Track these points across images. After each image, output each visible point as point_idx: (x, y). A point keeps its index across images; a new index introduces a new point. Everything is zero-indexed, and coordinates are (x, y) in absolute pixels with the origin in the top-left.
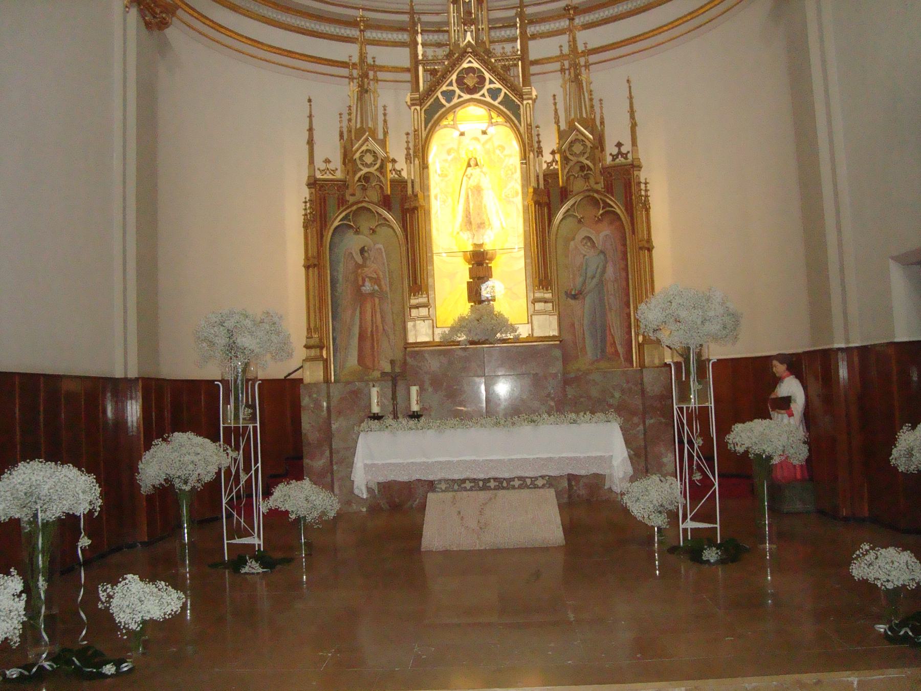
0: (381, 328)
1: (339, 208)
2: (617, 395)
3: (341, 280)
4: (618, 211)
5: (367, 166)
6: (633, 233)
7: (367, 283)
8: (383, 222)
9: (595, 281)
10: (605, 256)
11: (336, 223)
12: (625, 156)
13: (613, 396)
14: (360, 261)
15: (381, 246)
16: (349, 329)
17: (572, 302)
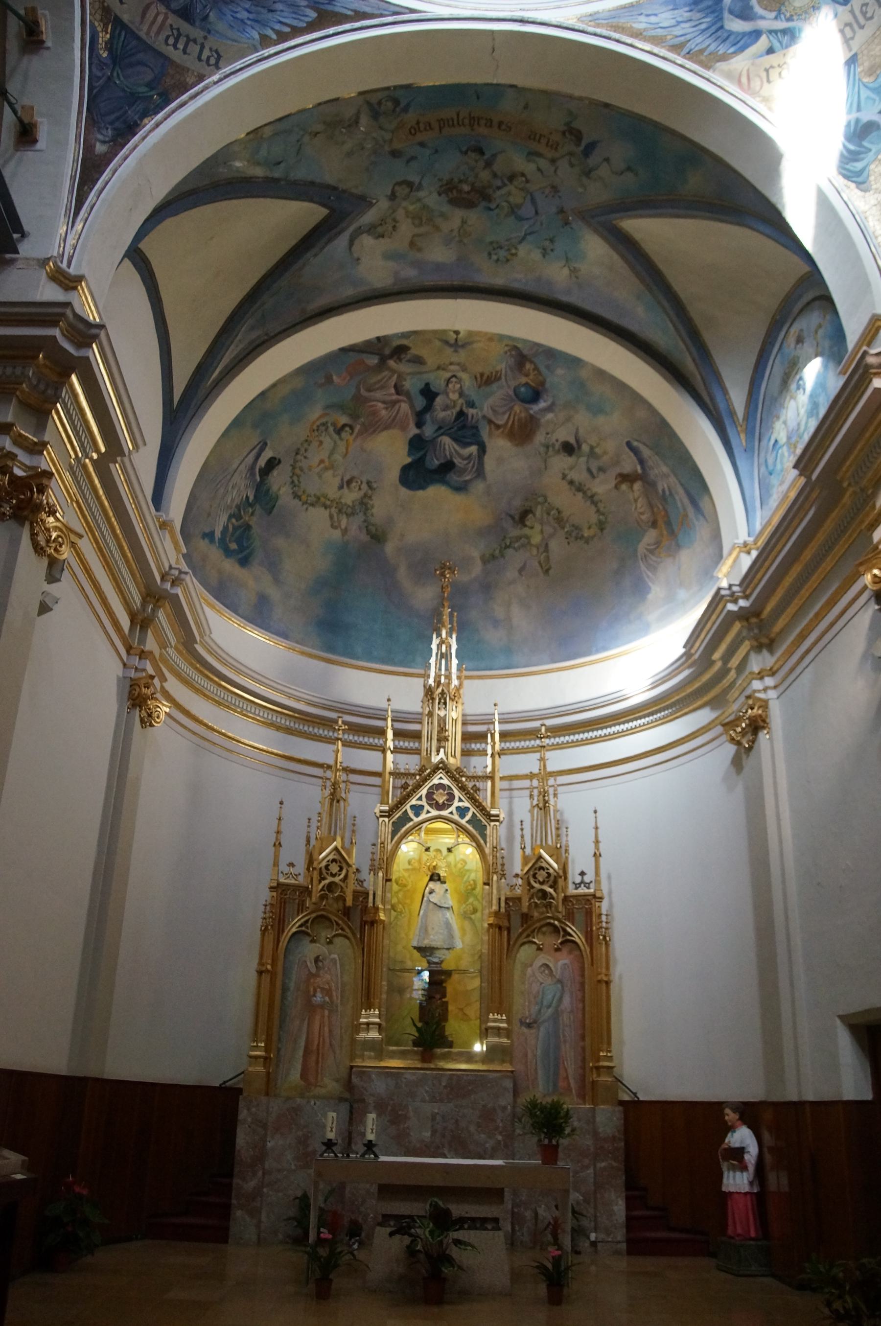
0: (327, 1040)
3: (292, 989)
6: (592, 965)
7: (319, 995)
9: (550, 1011)
11: (294, 930)
14: (314, 970)
15: (336, 956)
17: (525, 1030)
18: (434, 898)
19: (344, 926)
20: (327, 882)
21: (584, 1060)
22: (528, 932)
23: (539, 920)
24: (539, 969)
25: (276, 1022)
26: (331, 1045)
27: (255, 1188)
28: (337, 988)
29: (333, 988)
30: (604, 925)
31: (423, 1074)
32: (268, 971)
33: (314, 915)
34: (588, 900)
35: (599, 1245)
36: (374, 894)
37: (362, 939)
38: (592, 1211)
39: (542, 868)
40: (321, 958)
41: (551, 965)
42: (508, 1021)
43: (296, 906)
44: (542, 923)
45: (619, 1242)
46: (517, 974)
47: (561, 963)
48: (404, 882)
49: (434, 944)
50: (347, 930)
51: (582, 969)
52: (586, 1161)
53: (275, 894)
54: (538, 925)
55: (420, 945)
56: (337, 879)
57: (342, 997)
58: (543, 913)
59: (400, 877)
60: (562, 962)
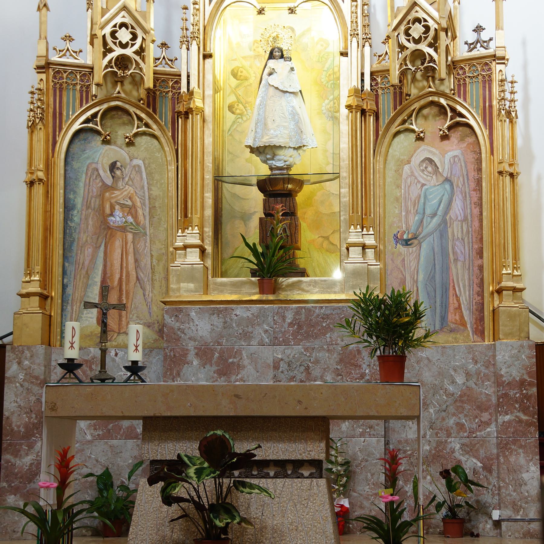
0: (133, 273)
1: (81, 106)
2: (460, 380)
3: (79, 206)
4: (472, 122)
5: (124, 46)
6: (492, 153)
7: (118, 213)
8: (144, 129)
9: (436, 220)
10: (452, 185)
11: (76, 126)
12: (485, 44)
13: (453, 382)
14: (109, 181)
15: (140, 162)
16: (88, 275)
17: (401, 248)
18: (274, 80)
19: (150, 122)
20: (114, 55)
21: (481, 284)
22: (404, 116)
23: (420, 98)
24: (421, 165)
25: (58, 252)
26: (137, 278)
27: (31, 464)
28: (143, 204)
29: (139, 204)
30: (508, 96)
31: (261, 309)
32: (40, 180)
33: (105, 106)
34: (486, 64)
35: (504, 525)
36: (188, 76)
37: (174, 137)
38: (494, 481)
39: (418, 20)
40: (119, 164)
41: (436, 160)
42: (378, 237)
43: (78, 95)
44: (422, 102)
45: (531, 521)
46: (390, 174)
47: (450, 154)
48: (245, 73)
49: (276, 141)
50: (155, 127)
51: (479, 161)
52: (485, 416)
53: (43, 76)
54: (417, 105)
55: (257, 144)
56: (129, 52)
57: (151, 216)
58: (424, 88)
59: (239, 68)
60: (451, 154)
